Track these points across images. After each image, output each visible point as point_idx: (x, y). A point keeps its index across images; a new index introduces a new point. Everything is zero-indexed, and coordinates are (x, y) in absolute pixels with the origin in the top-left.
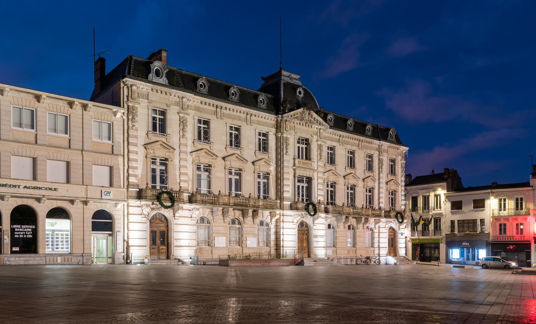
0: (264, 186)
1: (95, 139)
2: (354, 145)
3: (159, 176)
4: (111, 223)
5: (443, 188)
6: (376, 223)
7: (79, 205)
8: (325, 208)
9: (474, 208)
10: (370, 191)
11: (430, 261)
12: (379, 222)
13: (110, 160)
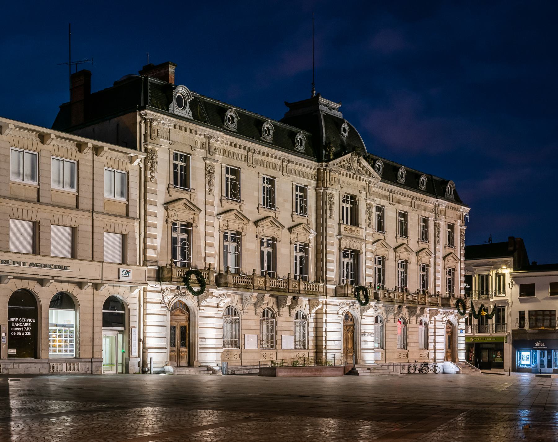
0: (301, 263)
1: (107, 195)
2: (405, 204)
3: (180, 248)
4: (123, 315)
5: (508, 266)
6: (432, 315)
7: (88, 289)
8: (375, 293)
9: (552, 294)
10: (379, 263)
11: (490, 369)
12: (436, 314)
13: (123, 224)
